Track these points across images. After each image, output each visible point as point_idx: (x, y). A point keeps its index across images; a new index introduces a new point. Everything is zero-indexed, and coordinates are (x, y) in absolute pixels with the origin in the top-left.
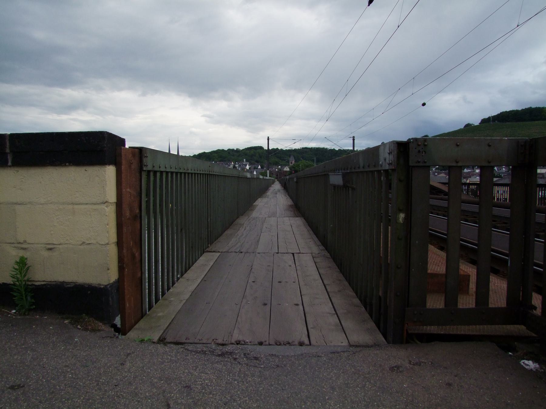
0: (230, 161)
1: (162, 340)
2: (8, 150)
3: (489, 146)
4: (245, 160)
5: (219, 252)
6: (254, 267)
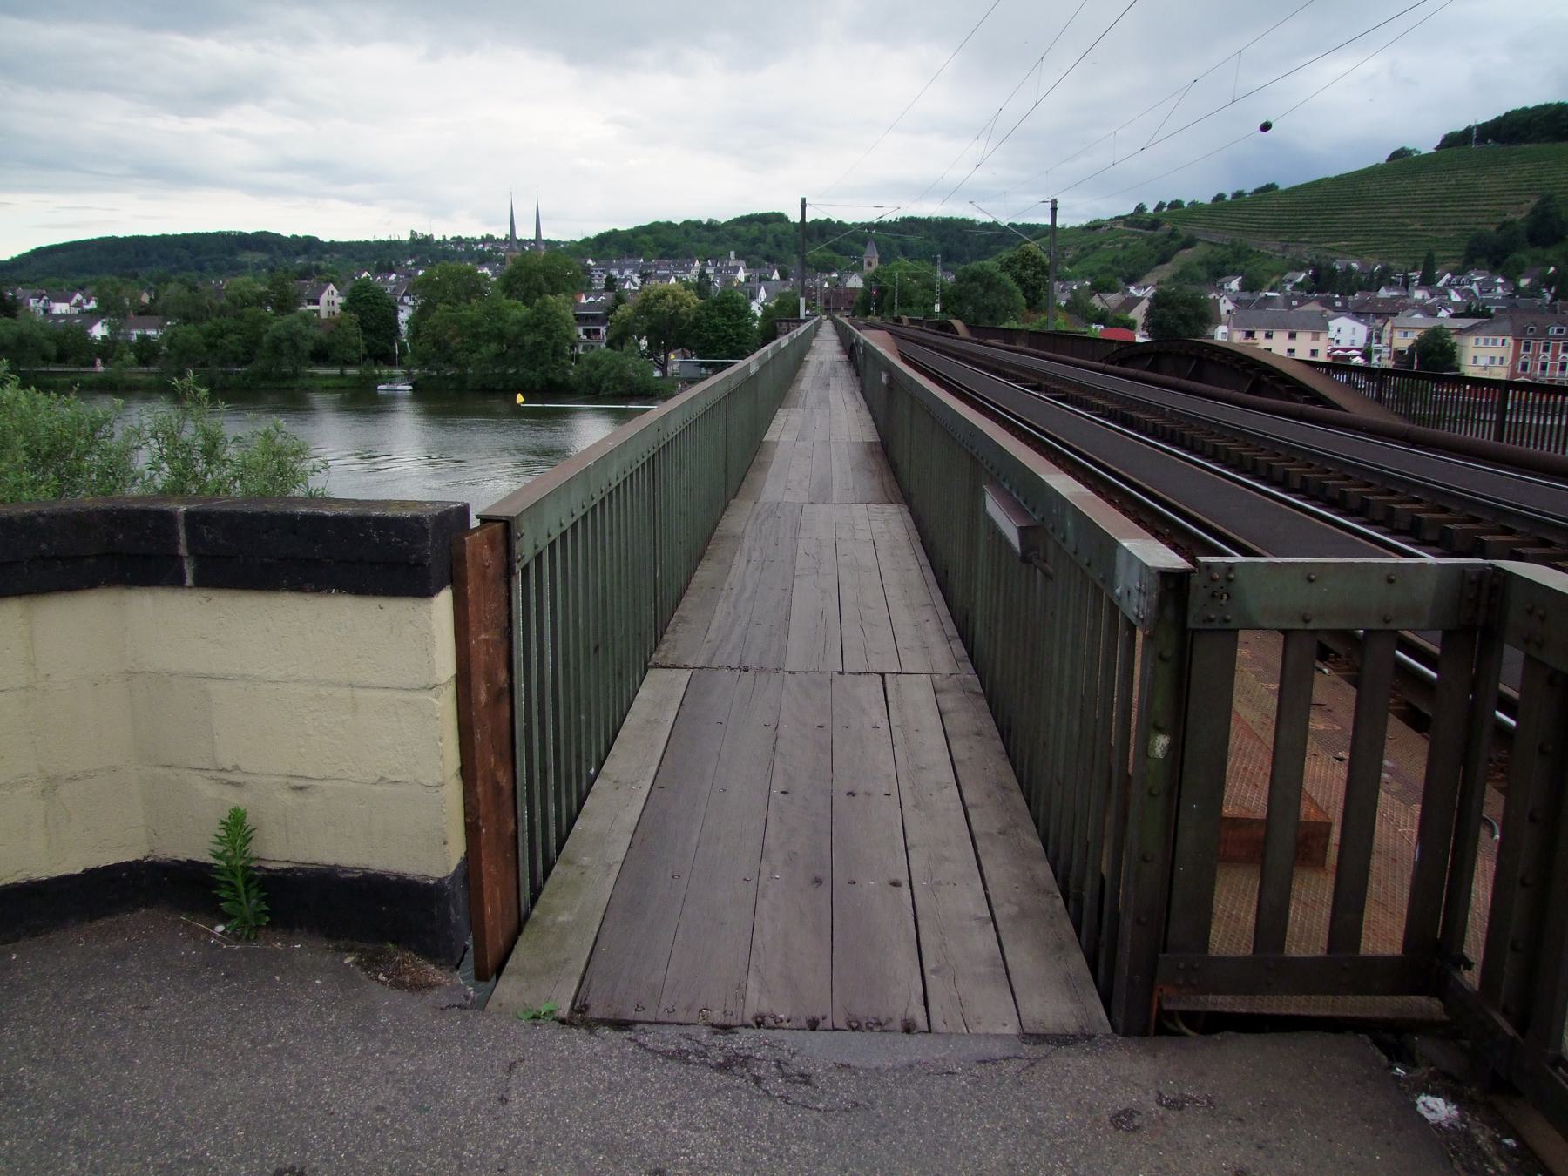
0: (690, 257)
1: (579, 1017)
2: (183, 551)
3: (1390, 581)
4: (732, 254)
5: (686, 667)
6: (781, 731)
